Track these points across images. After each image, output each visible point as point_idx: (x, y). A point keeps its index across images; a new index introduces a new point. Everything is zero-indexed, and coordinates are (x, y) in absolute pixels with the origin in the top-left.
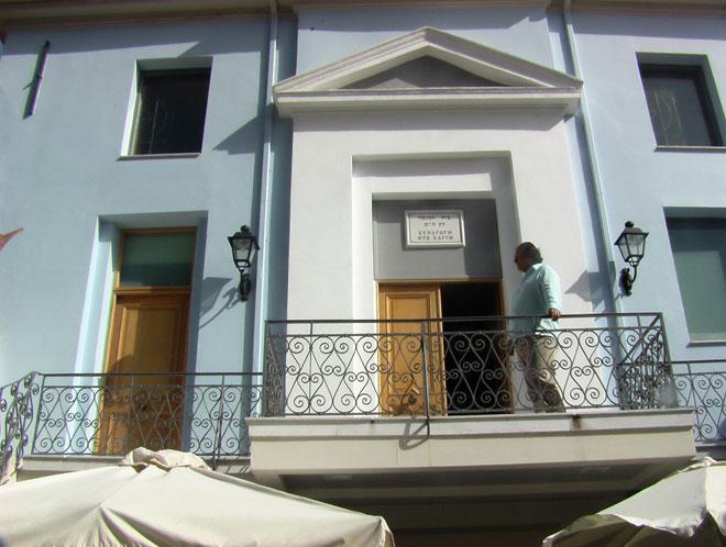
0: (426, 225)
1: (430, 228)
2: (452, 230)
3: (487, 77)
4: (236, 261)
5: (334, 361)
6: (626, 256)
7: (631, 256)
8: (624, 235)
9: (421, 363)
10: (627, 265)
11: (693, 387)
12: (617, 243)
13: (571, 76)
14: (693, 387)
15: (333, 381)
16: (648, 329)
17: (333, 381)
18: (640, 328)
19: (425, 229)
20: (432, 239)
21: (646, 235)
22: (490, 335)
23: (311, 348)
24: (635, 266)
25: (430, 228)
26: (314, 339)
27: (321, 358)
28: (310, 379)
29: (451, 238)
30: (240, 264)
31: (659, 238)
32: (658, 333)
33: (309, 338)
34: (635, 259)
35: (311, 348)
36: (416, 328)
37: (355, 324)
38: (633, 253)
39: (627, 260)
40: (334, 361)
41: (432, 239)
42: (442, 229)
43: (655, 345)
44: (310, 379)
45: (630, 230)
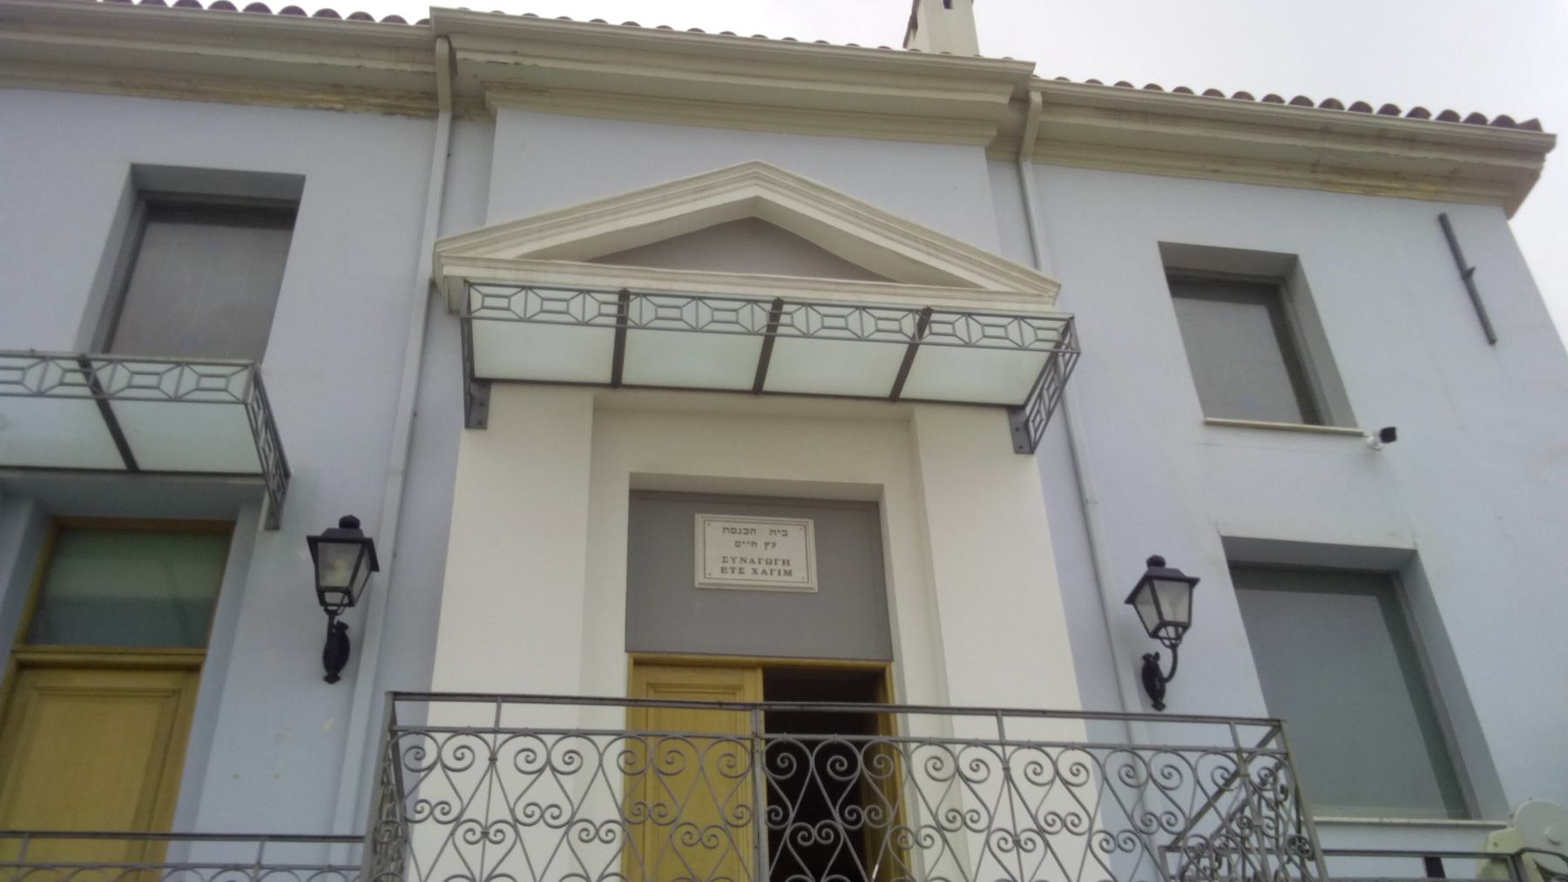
0: (738, 544)
1: (747, 551)
2: (787, 555)
3: (837, 252)
4: (321, 592)
5: (546, 790)
6: (1153, 622)
7: (1163, 624)
8: (1147, 580)
9: (750, 803)
10: (1155, 646)
11: (1008, 777)
12: (1131, 600)
13: (1032, 269)
14: (1008, 777)
15: (540, 839)
16: (1252, 754)
17: (540, 839)
18: (1239, 751)
19: (737, 553)
20: (748, 574)
21: (1192, 582)
22: (859, 745)
23: (493, 760)
24: (1174, 647)
25: (747, 551)
26: (502, 737)
27: (515, 783)
28: (485, 834)
29: (789, 573)
30: (329, 597)
31: (1217, 605)
32: (1278, 767)
33: (489, 737)
34: (1171, 631)
35: (493, 760)
36: (116, 851)
37: (956, 719)
38: (1168, 617)
39: (1154, 634)
40: (546, 790)
41: (748, 574)
42: (770, 554)
43: (1269, 795)
44: (485, 834)
45: (1157, 571)
